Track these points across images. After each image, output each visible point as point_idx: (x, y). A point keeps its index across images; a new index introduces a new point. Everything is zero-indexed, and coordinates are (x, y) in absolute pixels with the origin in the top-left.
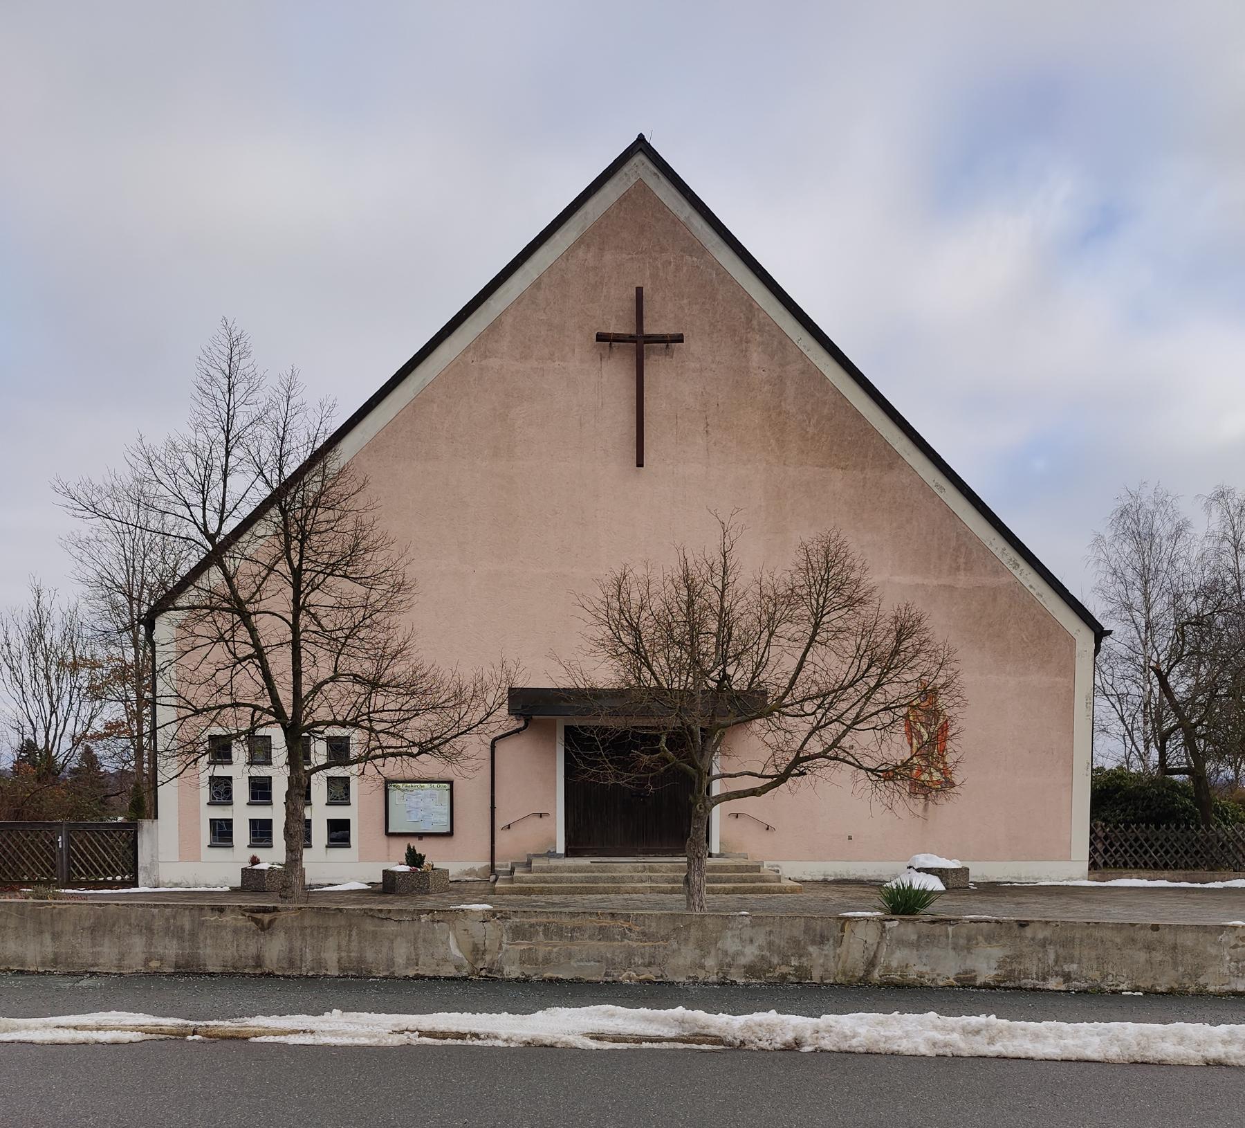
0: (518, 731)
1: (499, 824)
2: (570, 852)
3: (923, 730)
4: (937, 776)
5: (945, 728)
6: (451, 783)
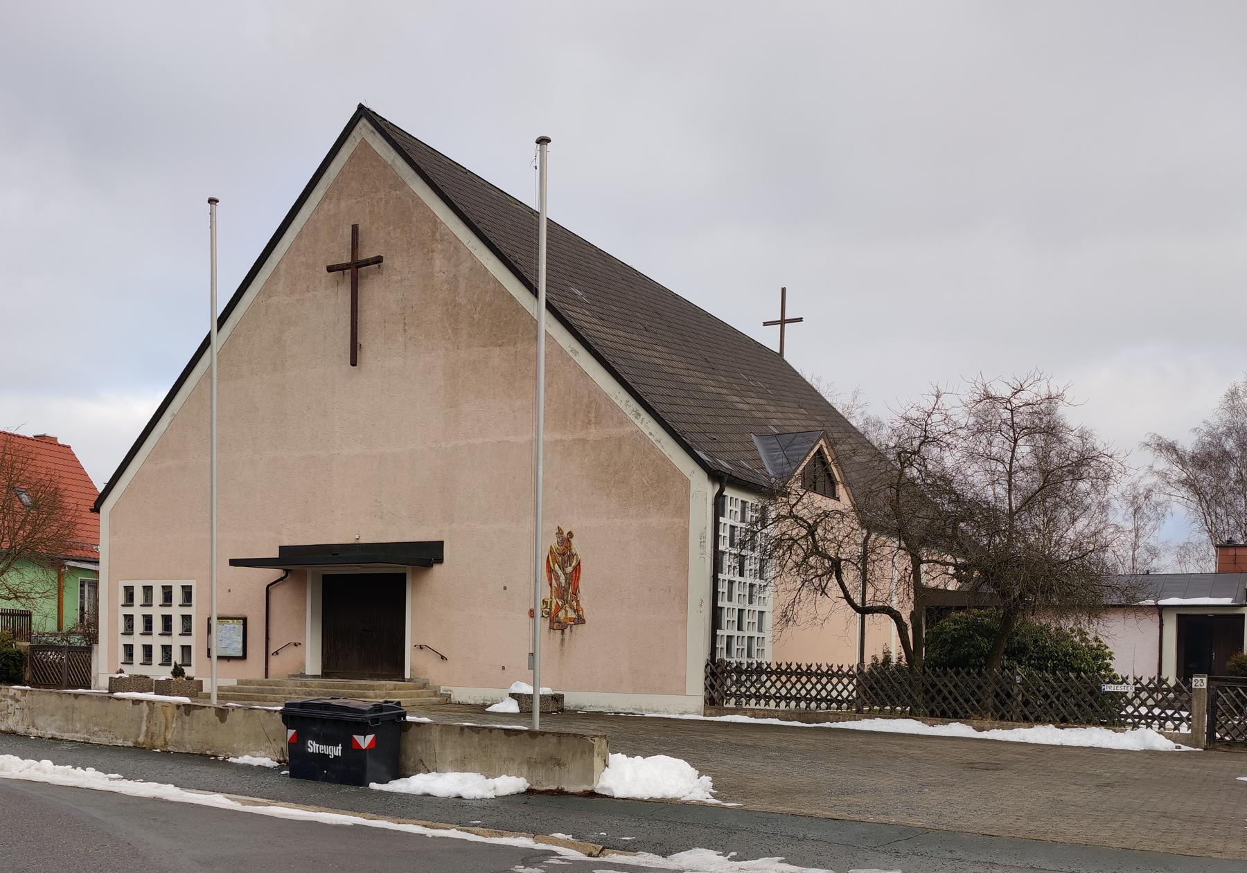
0: (281, 579)
1: (272, 650)
2: (326, 673)
3: (560, 572)
4: (572, 615)
5: (577, 569)
6: (245, 620)
